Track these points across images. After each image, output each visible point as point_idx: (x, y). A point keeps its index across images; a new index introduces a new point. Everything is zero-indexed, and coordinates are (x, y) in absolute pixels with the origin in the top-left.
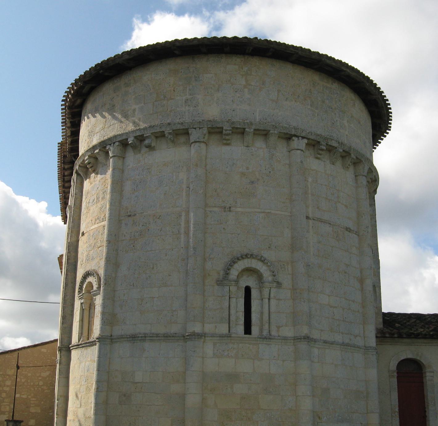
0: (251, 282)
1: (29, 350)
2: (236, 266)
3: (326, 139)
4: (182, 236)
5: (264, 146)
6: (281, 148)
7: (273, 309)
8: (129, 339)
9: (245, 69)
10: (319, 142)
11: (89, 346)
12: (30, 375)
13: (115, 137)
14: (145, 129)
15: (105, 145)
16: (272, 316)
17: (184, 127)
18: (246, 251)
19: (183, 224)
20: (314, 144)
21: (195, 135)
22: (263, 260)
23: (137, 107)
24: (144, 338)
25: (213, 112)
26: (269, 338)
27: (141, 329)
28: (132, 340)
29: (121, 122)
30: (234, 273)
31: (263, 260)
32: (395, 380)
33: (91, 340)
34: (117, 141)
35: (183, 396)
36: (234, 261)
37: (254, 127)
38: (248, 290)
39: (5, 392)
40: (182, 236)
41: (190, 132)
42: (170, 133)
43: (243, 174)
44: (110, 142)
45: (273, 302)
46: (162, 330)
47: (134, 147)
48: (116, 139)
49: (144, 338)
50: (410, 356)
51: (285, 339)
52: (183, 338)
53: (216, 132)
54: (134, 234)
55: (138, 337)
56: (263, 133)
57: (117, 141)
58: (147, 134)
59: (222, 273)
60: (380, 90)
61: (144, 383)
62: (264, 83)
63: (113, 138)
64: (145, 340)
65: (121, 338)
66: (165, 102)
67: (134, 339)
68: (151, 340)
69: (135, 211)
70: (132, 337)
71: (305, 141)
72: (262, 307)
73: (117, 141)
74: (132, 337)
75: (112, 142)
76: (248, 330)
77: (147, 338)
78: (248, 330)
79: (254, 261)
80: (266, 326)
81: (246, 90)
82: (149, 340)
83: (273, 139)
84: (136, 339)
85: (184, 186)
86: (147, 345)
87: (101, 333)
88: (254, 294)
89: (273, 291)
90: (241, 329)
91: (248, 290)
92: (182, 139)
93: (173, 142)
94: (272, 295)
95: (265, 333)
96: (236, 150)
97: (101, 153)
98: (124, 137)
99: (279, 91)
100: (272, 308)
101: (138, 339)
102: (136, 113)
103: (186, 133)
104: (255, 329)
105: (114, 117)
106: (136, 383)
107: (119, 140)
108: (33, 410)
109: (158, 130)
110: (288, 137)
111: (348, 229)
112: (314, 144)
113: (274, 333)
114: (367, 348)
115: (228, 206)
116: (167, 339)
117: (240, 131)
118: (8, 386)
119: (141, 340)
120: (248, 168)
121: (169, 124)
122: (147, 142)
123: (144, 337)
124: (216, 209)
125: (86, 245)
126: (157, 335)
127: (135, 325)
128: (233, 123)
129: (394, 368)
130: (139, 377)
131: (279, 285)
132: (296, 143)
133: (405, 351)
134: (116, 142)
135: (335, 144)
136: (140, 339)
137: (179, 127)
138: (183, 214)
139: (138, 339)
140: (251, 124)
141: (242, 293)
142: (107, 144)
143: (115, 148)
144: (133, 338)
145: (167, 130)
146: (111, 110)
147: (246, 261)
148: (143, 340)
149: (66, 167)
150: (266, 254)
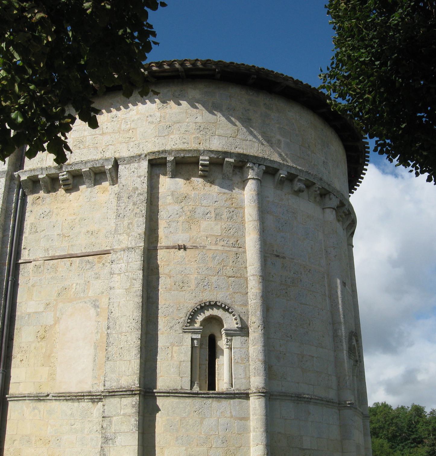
8: (293, 399)
11: (225, 398)
13: (263, 160)
14: (301, 171)
15: (247, 161)
17: (328, 189)
24: (310, 400)
27: (306, 390)
28: (297, 400)
29: (263, 144)
34: (265, 165)
44: (255, 161)
48: (264, 162)
49: (310, 400)
52: (337, 405)
54: (285, 279)
55: (305, 398)
57: (265, 165)
58: (303, 177)
60: (71, 125)
61: (313, 450)
63: (261, 159)
64: (310, 402)
67: (299, 399)
68: (315, 402)
69: (283, 253)
70: (298, 397)
73: (264, 164)
74: (298, 397)
75: (258, 163)
77: (312, 400)
82: (256, 395)
84: (302, 399)
87: (265, 386)
101: (304, 400)
105: (251, 133)
106: (304, 449)
107: (268, 165)
116: (328, 404)
119: (307, 401)
123: (309, 401)
127: (298, 383)
134: (263, 165)
136: (306, 400)
139: (304, 400)
142: (250, 161)
143: (261, 171)
145: (318, 185)
146: (247, 122)
148: (308, 401)
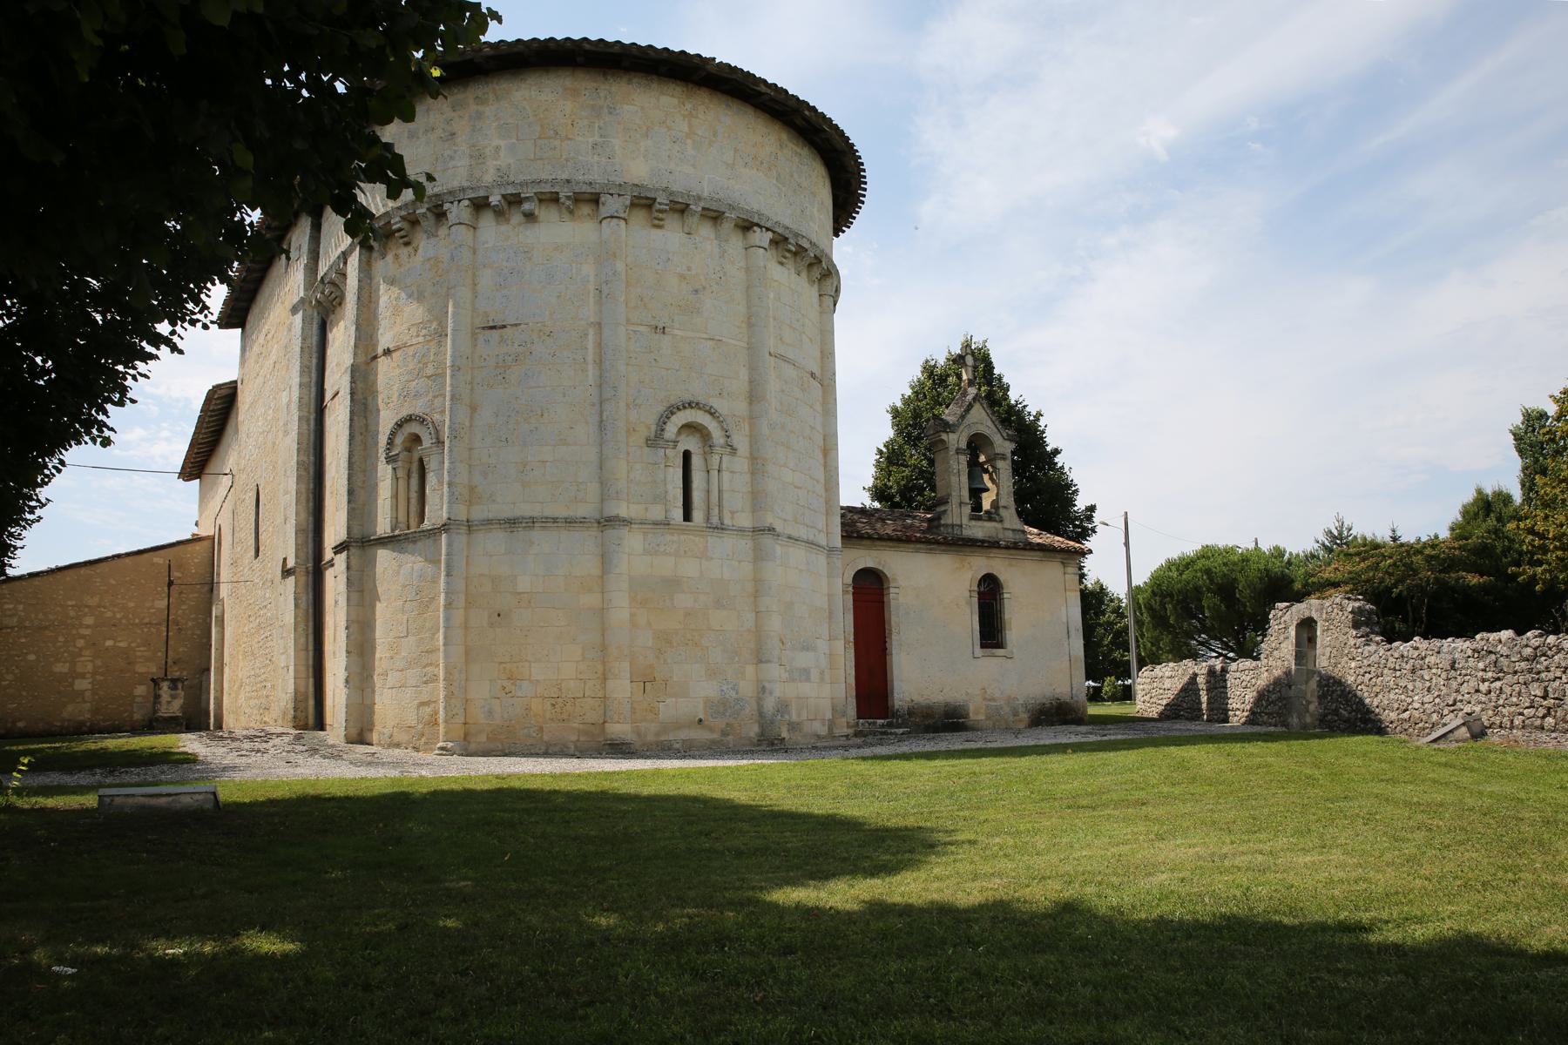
0: (691, 443)
1: (127, 560)
2: (674, 418)
3: (797, 235)
4: (590, 367)
5: (712, 236)
6: (736, 242)
7: (726, 486)
9: (689, 106)
10: (786, 239)
12: (131, 605)
16: (726, 496)
18: (687, 398)
19: (590, 346)
20: (779, 241)
21: (611, 205)
22: (712, 413)
23: (502, 143)
25: (638, 170)
26: (721, 528)
30: (671, 430)
31: (712, 413)
32: (850, 597)
33: (427, 525)
35: (602, 612)
36: (672, 410)
37: (702, 204)
38: (687, 456)
39: (83, 637)
40: (590, 367)
41: (602, 199)
42: (568, 198)
43: (682, 277)
45: (726, 475)
46: (562, 512)
47: (499, 213)
50: (870, 564)
51: (741, 530)
53: (644, 203)
56: (714, 216)
59: (653, 428)
62: (715, 135)
65: (488, 523)
66: (557, 143)
71: (770, 235)
72: (708, 482)
76: (687, 516)
78: (687, 516)
79: (700, 413)
80: (716, 511)
81: (689, 141)
83: (727, 226)
85: (591, 287)
86: (536, 534)
88: (696, 462)
89: (725, 458)
90: (678, 513)
91: (687, 456)
92: (586, 209)
93: (571, 212)
94: (724, 466)
95: (715, 520)
96: (671, 236)
97: (429, 215)
98: (482, 193)
99: (736, 150)
100: (727, 482)
102: (502, 154)
103: (595, 200)
104: (698, 515)
108: (141, 669)
109: (547, 189)
110: (746, 226)
111: (812, 374)
112: (779, 241)
113: (727, 521)
114: (831, 550)
115: (661, 325)
117: (681, 209)
118: (88, 627)
120: (689, 269)
121: (568, 181)
122: (526, 206)
123: (532, 522)
124: (641, 328)
125: (397, 372)
126: (555, 520)
128: (672, 193)
129: (850, 581)
130: (524, 584)
131: (734, 450)
132: (761, 238)
133: (866, 558)
135: (806, 245)
137: (586, 189)
138: (591, 332)
140: (699, 198)
141: (680, 461)
144: (512, 523)
147: (688, 411)
149: (275, 224)
150: (715, 403)
